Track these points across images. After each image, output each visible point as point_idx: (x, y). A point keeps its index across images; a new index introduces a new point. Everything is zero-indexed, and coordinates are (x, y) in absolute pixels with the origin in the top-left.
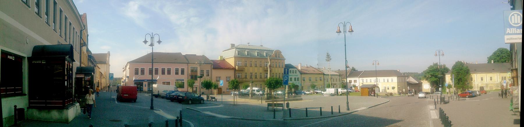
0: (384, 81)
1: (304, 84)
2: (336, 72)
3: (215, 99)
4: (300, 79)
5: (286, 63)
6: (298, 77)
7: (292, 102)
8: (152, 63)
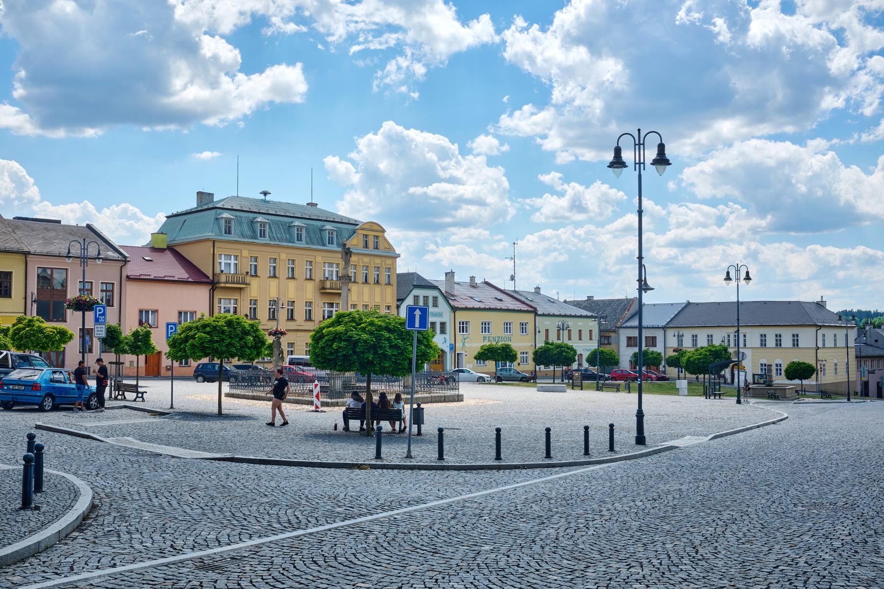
0: (763, 343)
1: (464, 345)
2: (577, 304)
3: (138, 392)
4: (449, 328)
5: (397, 272)
6: (443, 320)
7: (429, 405)
8: (847, 347)
